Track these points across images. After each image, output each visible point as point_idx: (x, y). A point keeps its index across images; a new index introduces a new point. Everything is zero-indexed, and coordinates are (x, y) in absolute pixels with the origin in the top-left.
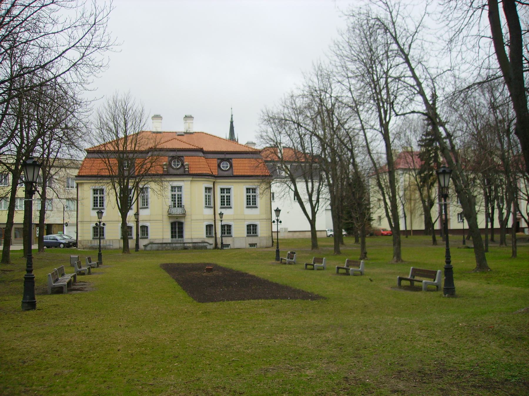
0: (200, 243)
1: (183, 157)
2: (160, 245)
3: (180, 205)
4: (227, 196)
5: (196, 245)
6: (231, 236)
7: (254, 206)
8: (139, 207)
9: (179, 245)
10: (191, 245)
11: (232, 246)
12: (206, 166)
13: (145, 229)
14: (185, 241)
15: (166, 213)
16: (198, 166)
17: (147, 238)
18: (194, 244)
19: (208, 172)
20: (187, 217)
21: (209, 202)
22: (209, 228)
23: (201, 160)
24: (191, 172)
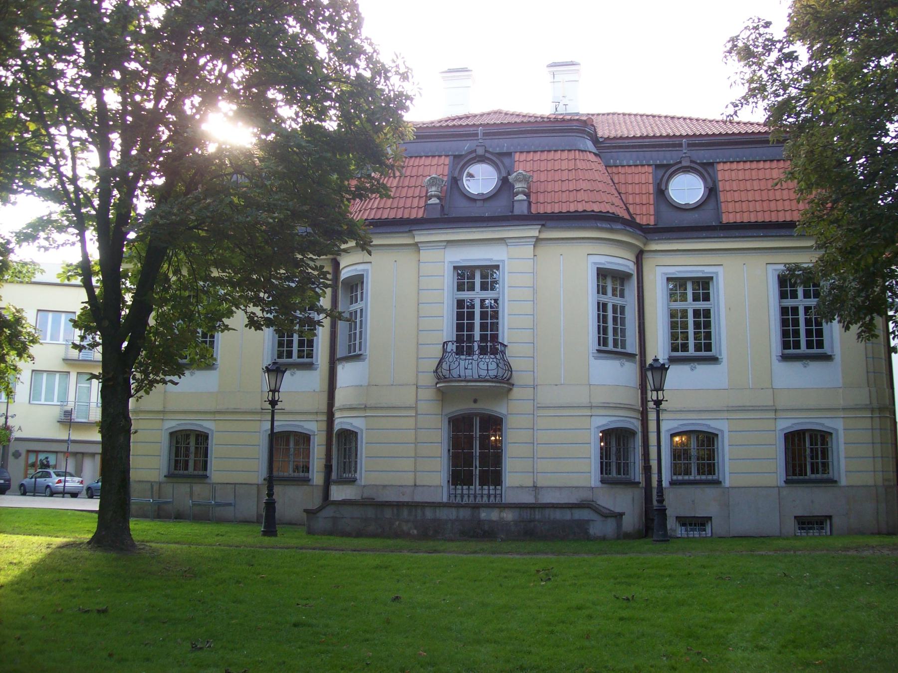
2: (370, 512)
3: (492, 344)
4: (696, 313)
5: (538, 515)
6: (718, 483)
8: (340, 353)
9: (452, 514)
11: (717, 526)
12: (601, 186)
13: (345, 441)
14: (510, 497)
15: (428, 379)
17: (353, 481)
18: (526, 514)
19: (612, 209)
20: (516, 392)
22: (616, 441)
23: (580, 165)
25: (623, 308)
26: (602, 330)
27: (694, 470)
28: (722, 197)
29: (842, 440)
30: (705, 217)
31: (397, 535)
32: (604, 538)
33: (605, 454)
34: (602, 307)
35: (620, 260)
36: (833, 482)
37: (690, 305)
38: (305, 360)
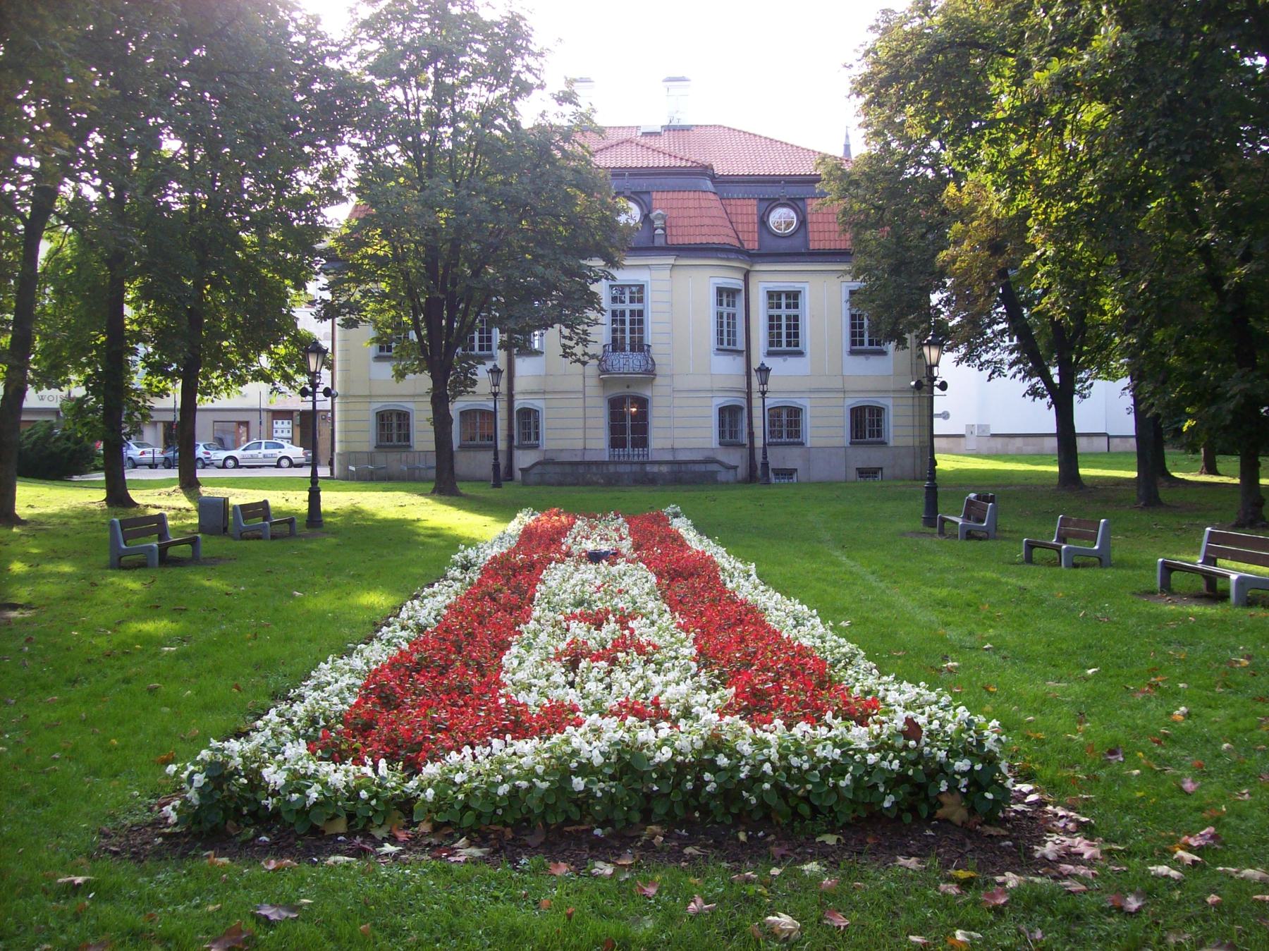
0: (694, 462)
1: (648, 193)
2: (568, 469)
3: (639, 346)
5: (683, 468)
6: (802, 444)
7: (731, 347)
9: (627, 468)
10: (664, 469)
12: (719, 222)
14: (654, 456)
16: (697, 222)
17: (537, 447)
18: (676, 468)
19: (727, 240)
20: (658, 380)
21: (731, 333)
22: (729, 416)
23: (703, 204)
24: (674, 240)
25: (734, 315)
26: (720, 333)
27: (785, 435)
28: (810, 227)
29: (891, 413)
30: (796, 243)
31: (588, 484)
32: (727, 483)
33: (722, 423)
34: (720, 315)
35: (733, 280)
36: (884, 443)
37: (784, 312)
38: (485, 352)
